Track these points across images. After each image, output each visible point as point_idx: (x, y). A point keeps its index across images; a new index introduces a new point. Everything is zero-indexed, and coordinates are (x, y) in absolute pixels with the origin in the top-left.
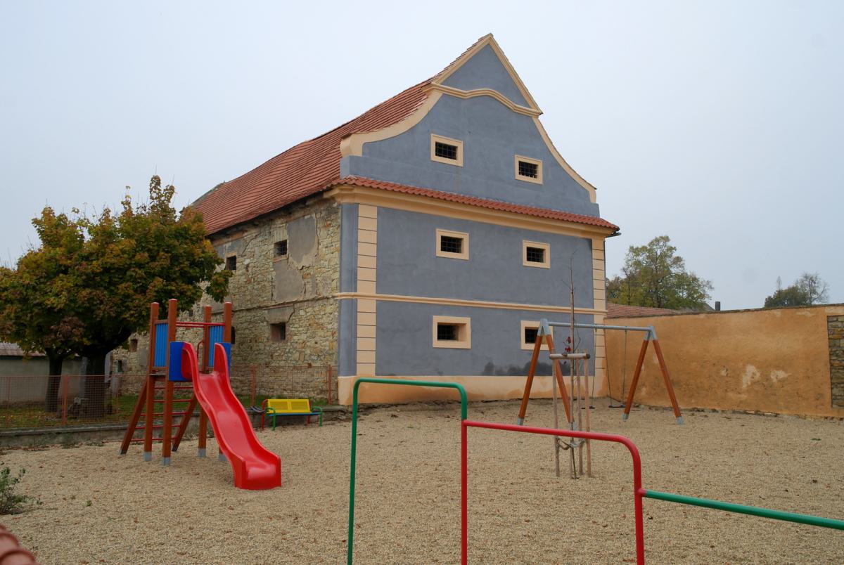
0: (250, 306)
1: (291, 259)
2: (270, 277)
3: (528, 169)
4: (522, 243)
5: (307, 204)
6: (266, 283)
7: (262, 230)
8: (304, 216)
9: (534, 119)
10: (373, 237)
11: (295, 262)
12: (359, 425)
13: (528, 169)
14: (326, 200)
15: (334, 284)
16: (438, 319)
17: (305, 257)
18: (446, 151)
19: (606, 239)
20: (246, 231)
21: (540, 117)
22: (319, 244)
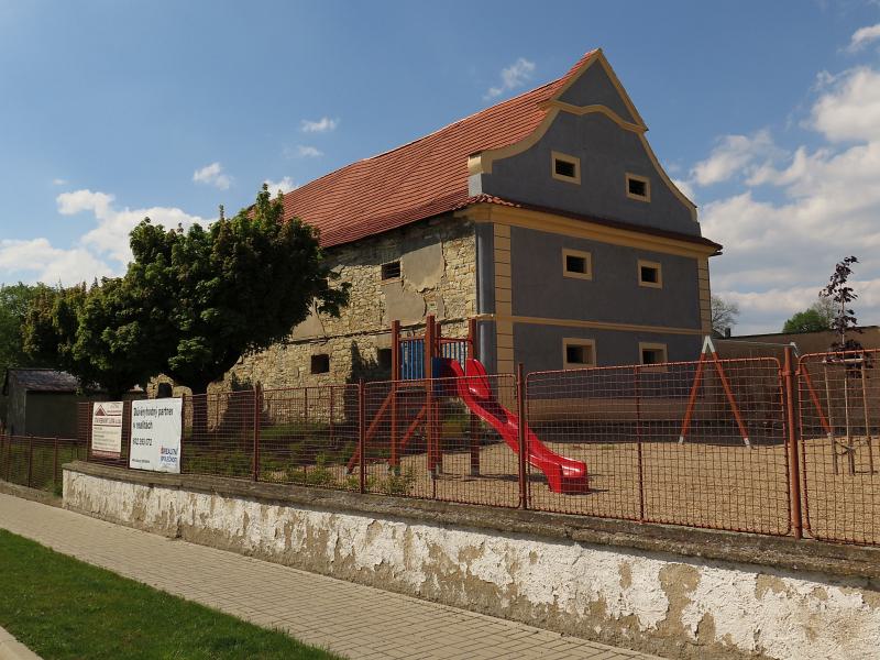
0: (349, 332)
1: (406, 281)
2: (377, 301)
3: (637, 187)
4: (561, 252)
5: (431, 223)
6: (371, 307)
7: (364, 252)
8: (423, 237)
9: (640, 135)
10: (508, 257)
11: (413, 285)
12: (482, 456)
13: (637, 187)
14: (456, 220)
15: (469, 306)
16: (567, 341)
17: (426, 279)
18: (565, 169)
19: (710, 259)
20: (341, 254)
21: (646, 134)
22: (446, 265)
